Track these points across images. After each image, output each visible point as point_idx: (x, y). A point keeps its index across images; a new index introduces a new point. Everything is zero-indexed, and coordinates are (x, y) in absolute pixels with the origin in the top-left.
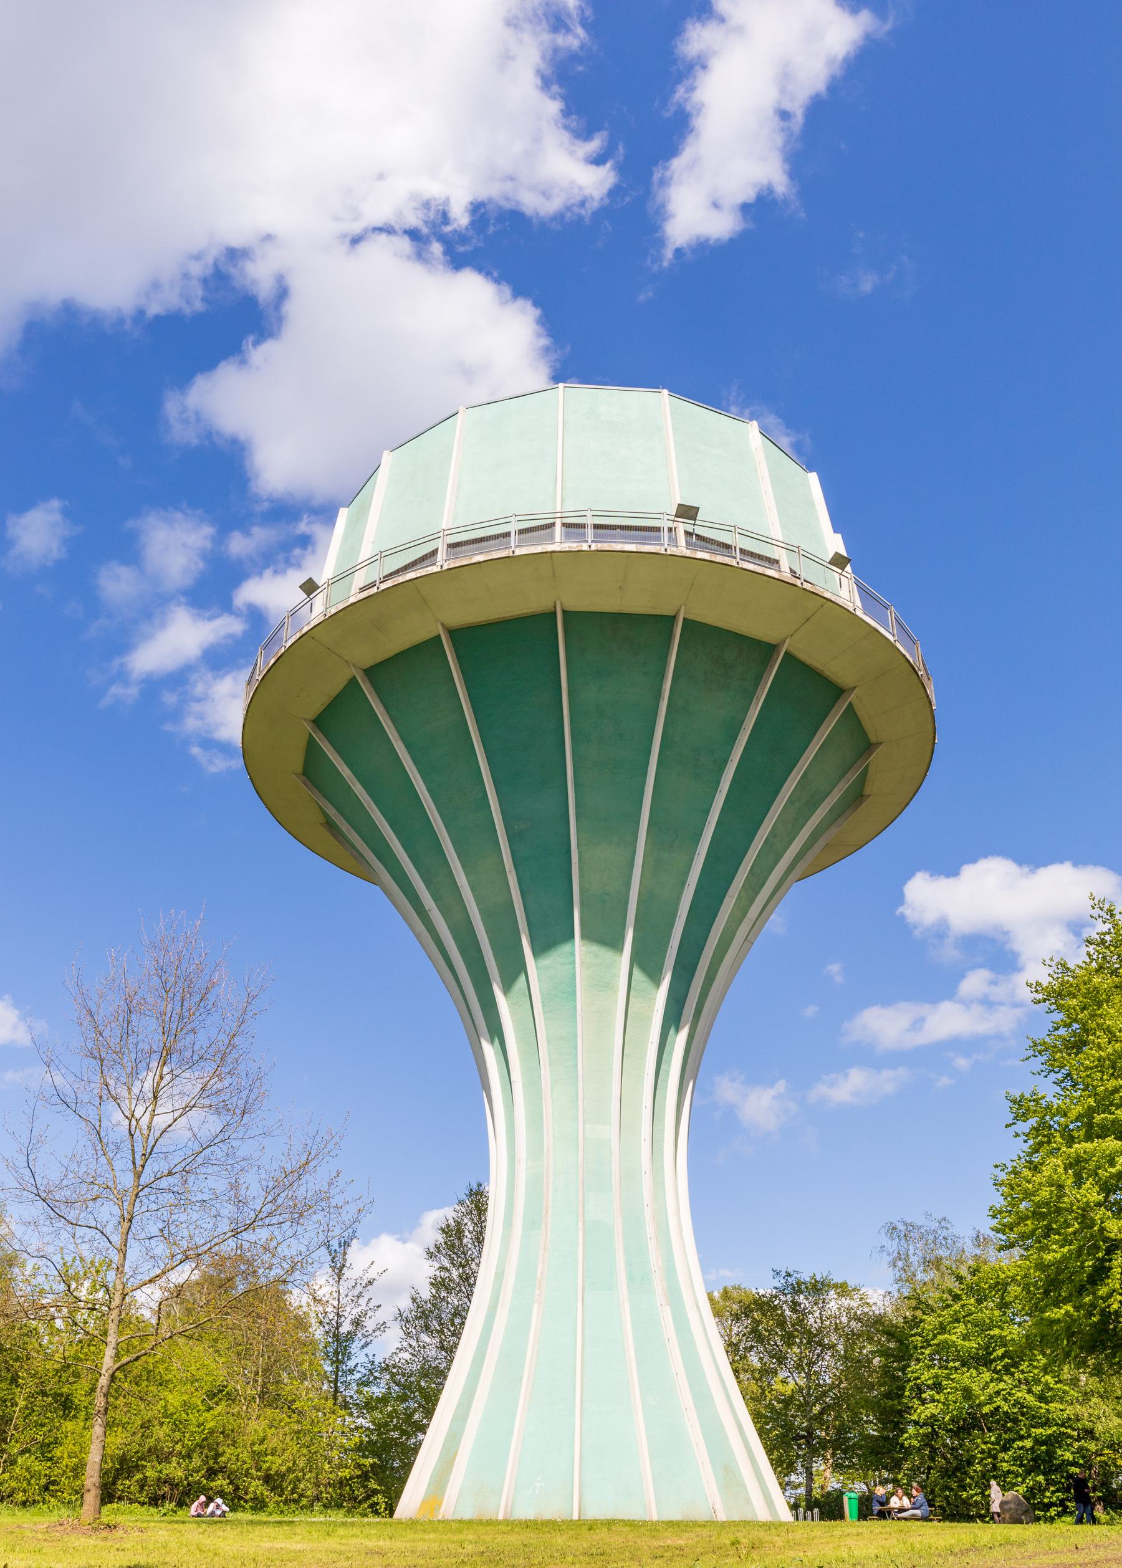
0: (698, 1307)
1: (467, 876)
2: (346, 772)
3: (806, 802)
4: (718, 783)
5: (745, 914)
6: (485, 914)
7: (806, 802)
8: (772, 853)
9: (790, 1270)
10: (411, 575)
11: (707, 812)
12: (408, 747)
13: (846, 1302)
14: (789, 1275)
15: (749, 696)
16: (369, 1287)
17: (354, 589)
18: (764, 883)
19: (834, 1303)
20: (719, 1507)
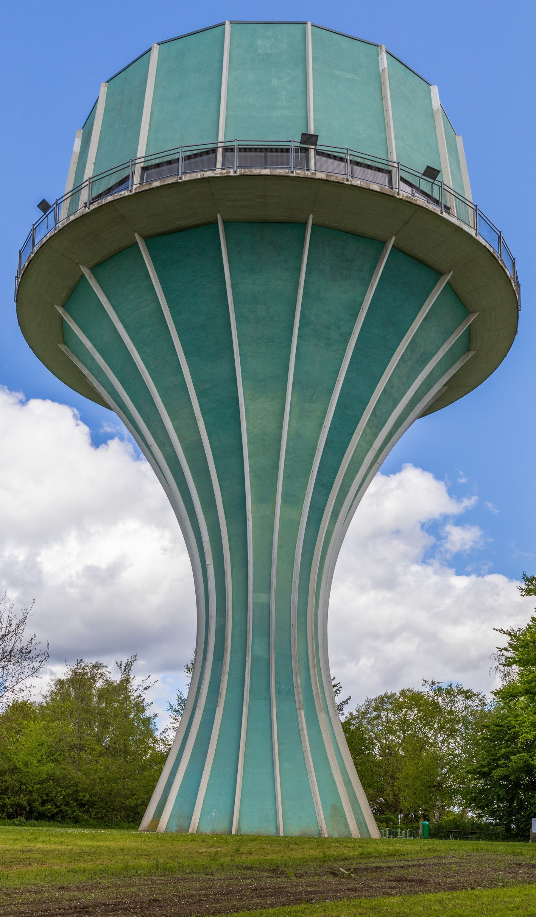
0: (327, 709)
1: (172, 421)
2: (88, 344)
3: (417, 358)
4: (345, 351)
5: (371, 445)
6: (185, 448)
7: (417, 358)
8: (391, 397)
9: (436, 680)
10: (110, 198)
11: (337, 372)
12: (126, 327)
13: (469, 702)
14: (433, 683)
15: (367, 284)
16: (146, 691)
17: (81, 205)
18: (385, 422)
19: (461, 703)
20: (324, 827)
